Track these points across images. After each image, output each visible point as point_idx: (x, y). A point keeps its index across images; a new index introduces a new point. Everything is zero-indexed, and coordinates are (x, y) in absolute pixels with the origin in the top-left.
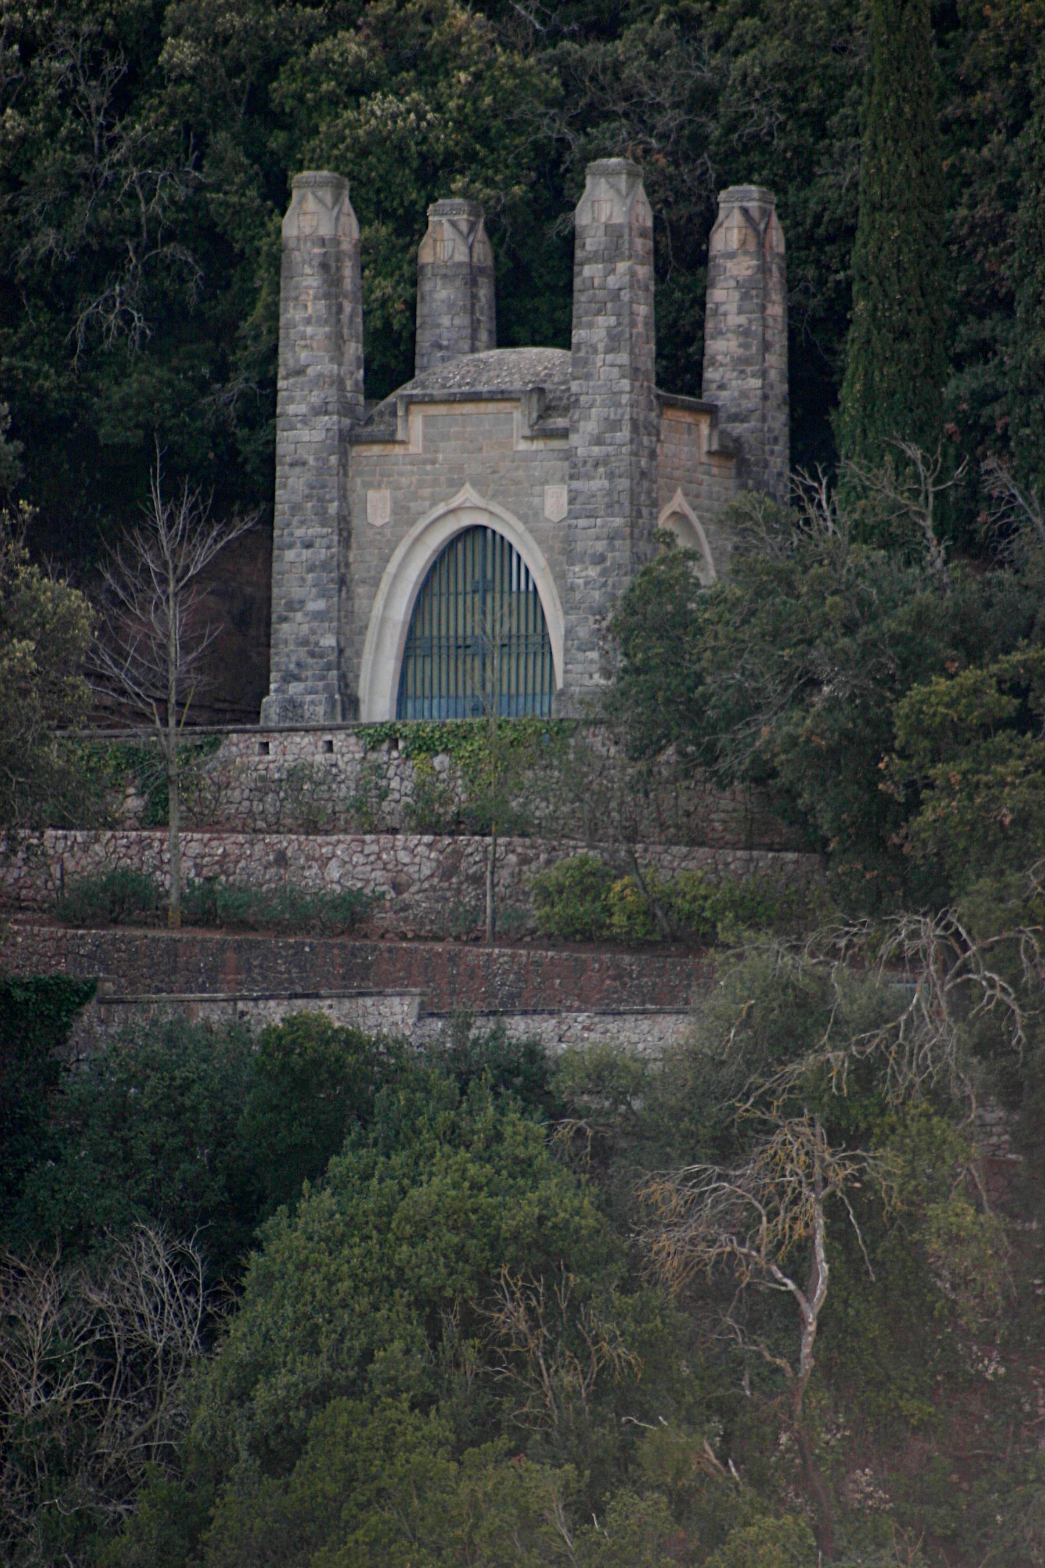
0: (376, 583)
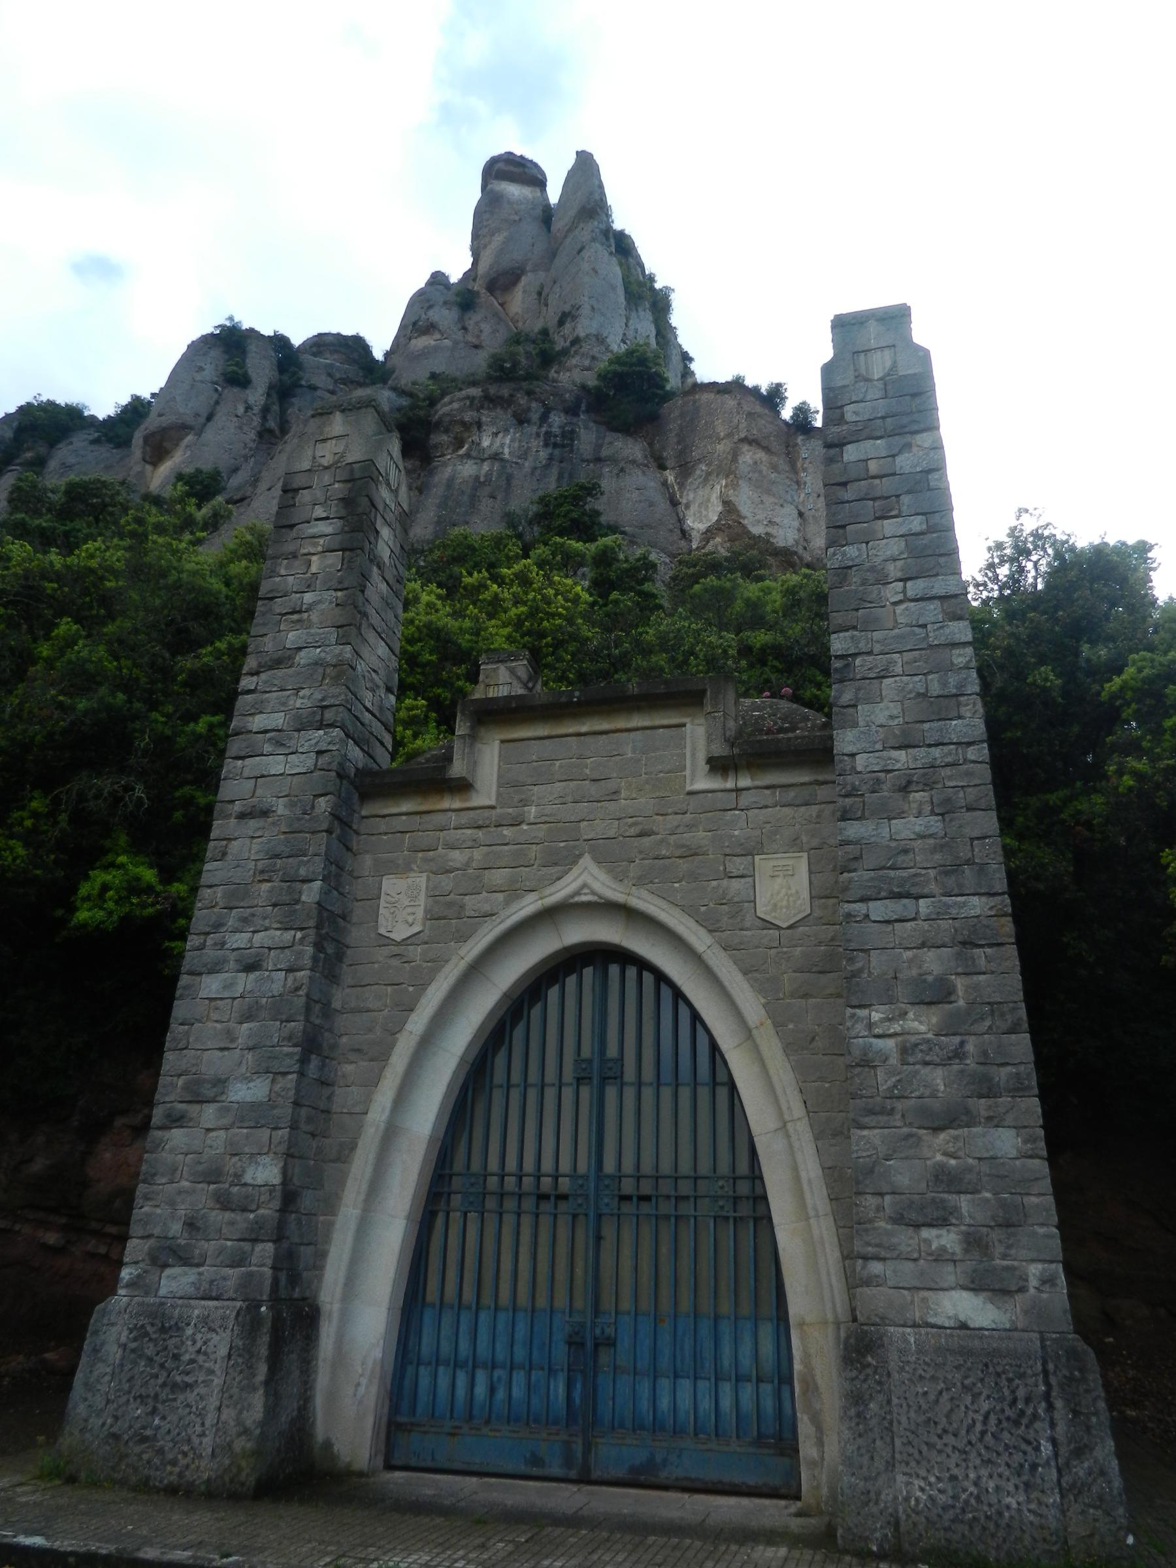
0: (382, 1056)
